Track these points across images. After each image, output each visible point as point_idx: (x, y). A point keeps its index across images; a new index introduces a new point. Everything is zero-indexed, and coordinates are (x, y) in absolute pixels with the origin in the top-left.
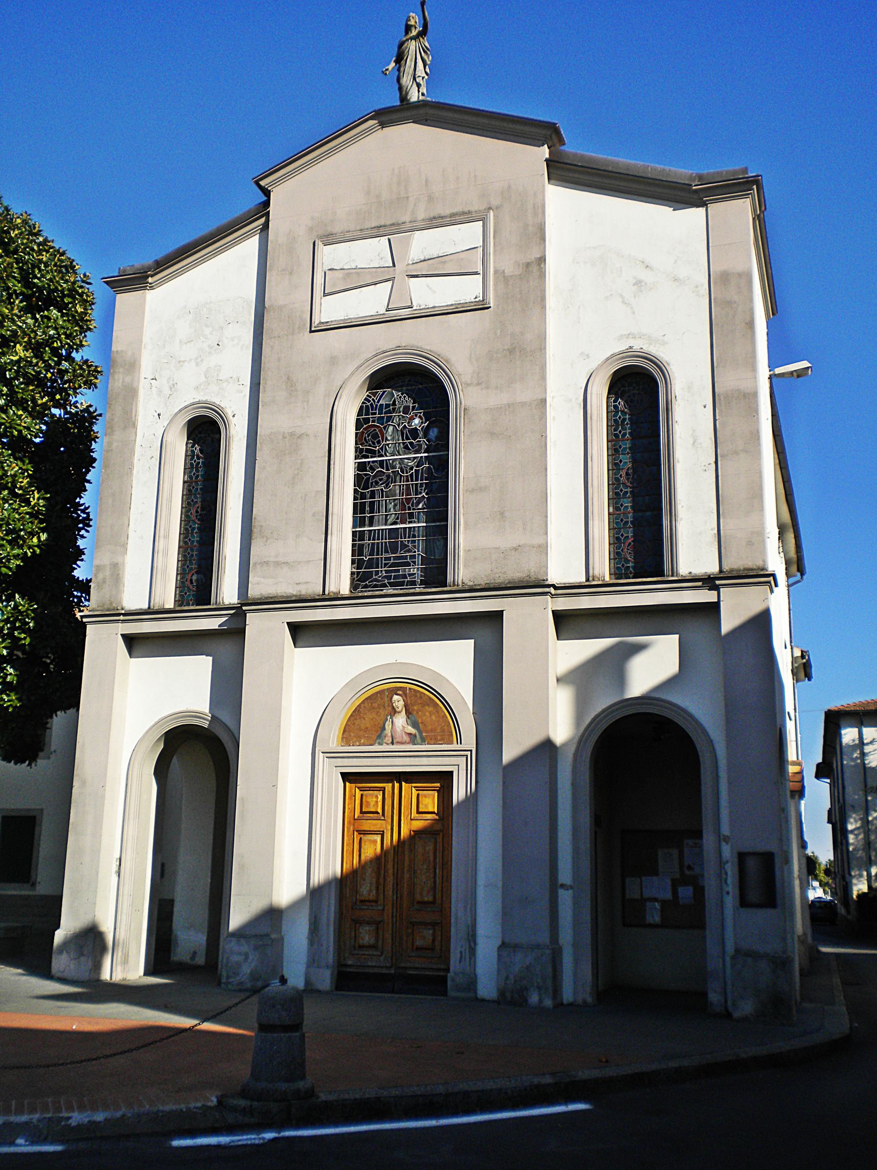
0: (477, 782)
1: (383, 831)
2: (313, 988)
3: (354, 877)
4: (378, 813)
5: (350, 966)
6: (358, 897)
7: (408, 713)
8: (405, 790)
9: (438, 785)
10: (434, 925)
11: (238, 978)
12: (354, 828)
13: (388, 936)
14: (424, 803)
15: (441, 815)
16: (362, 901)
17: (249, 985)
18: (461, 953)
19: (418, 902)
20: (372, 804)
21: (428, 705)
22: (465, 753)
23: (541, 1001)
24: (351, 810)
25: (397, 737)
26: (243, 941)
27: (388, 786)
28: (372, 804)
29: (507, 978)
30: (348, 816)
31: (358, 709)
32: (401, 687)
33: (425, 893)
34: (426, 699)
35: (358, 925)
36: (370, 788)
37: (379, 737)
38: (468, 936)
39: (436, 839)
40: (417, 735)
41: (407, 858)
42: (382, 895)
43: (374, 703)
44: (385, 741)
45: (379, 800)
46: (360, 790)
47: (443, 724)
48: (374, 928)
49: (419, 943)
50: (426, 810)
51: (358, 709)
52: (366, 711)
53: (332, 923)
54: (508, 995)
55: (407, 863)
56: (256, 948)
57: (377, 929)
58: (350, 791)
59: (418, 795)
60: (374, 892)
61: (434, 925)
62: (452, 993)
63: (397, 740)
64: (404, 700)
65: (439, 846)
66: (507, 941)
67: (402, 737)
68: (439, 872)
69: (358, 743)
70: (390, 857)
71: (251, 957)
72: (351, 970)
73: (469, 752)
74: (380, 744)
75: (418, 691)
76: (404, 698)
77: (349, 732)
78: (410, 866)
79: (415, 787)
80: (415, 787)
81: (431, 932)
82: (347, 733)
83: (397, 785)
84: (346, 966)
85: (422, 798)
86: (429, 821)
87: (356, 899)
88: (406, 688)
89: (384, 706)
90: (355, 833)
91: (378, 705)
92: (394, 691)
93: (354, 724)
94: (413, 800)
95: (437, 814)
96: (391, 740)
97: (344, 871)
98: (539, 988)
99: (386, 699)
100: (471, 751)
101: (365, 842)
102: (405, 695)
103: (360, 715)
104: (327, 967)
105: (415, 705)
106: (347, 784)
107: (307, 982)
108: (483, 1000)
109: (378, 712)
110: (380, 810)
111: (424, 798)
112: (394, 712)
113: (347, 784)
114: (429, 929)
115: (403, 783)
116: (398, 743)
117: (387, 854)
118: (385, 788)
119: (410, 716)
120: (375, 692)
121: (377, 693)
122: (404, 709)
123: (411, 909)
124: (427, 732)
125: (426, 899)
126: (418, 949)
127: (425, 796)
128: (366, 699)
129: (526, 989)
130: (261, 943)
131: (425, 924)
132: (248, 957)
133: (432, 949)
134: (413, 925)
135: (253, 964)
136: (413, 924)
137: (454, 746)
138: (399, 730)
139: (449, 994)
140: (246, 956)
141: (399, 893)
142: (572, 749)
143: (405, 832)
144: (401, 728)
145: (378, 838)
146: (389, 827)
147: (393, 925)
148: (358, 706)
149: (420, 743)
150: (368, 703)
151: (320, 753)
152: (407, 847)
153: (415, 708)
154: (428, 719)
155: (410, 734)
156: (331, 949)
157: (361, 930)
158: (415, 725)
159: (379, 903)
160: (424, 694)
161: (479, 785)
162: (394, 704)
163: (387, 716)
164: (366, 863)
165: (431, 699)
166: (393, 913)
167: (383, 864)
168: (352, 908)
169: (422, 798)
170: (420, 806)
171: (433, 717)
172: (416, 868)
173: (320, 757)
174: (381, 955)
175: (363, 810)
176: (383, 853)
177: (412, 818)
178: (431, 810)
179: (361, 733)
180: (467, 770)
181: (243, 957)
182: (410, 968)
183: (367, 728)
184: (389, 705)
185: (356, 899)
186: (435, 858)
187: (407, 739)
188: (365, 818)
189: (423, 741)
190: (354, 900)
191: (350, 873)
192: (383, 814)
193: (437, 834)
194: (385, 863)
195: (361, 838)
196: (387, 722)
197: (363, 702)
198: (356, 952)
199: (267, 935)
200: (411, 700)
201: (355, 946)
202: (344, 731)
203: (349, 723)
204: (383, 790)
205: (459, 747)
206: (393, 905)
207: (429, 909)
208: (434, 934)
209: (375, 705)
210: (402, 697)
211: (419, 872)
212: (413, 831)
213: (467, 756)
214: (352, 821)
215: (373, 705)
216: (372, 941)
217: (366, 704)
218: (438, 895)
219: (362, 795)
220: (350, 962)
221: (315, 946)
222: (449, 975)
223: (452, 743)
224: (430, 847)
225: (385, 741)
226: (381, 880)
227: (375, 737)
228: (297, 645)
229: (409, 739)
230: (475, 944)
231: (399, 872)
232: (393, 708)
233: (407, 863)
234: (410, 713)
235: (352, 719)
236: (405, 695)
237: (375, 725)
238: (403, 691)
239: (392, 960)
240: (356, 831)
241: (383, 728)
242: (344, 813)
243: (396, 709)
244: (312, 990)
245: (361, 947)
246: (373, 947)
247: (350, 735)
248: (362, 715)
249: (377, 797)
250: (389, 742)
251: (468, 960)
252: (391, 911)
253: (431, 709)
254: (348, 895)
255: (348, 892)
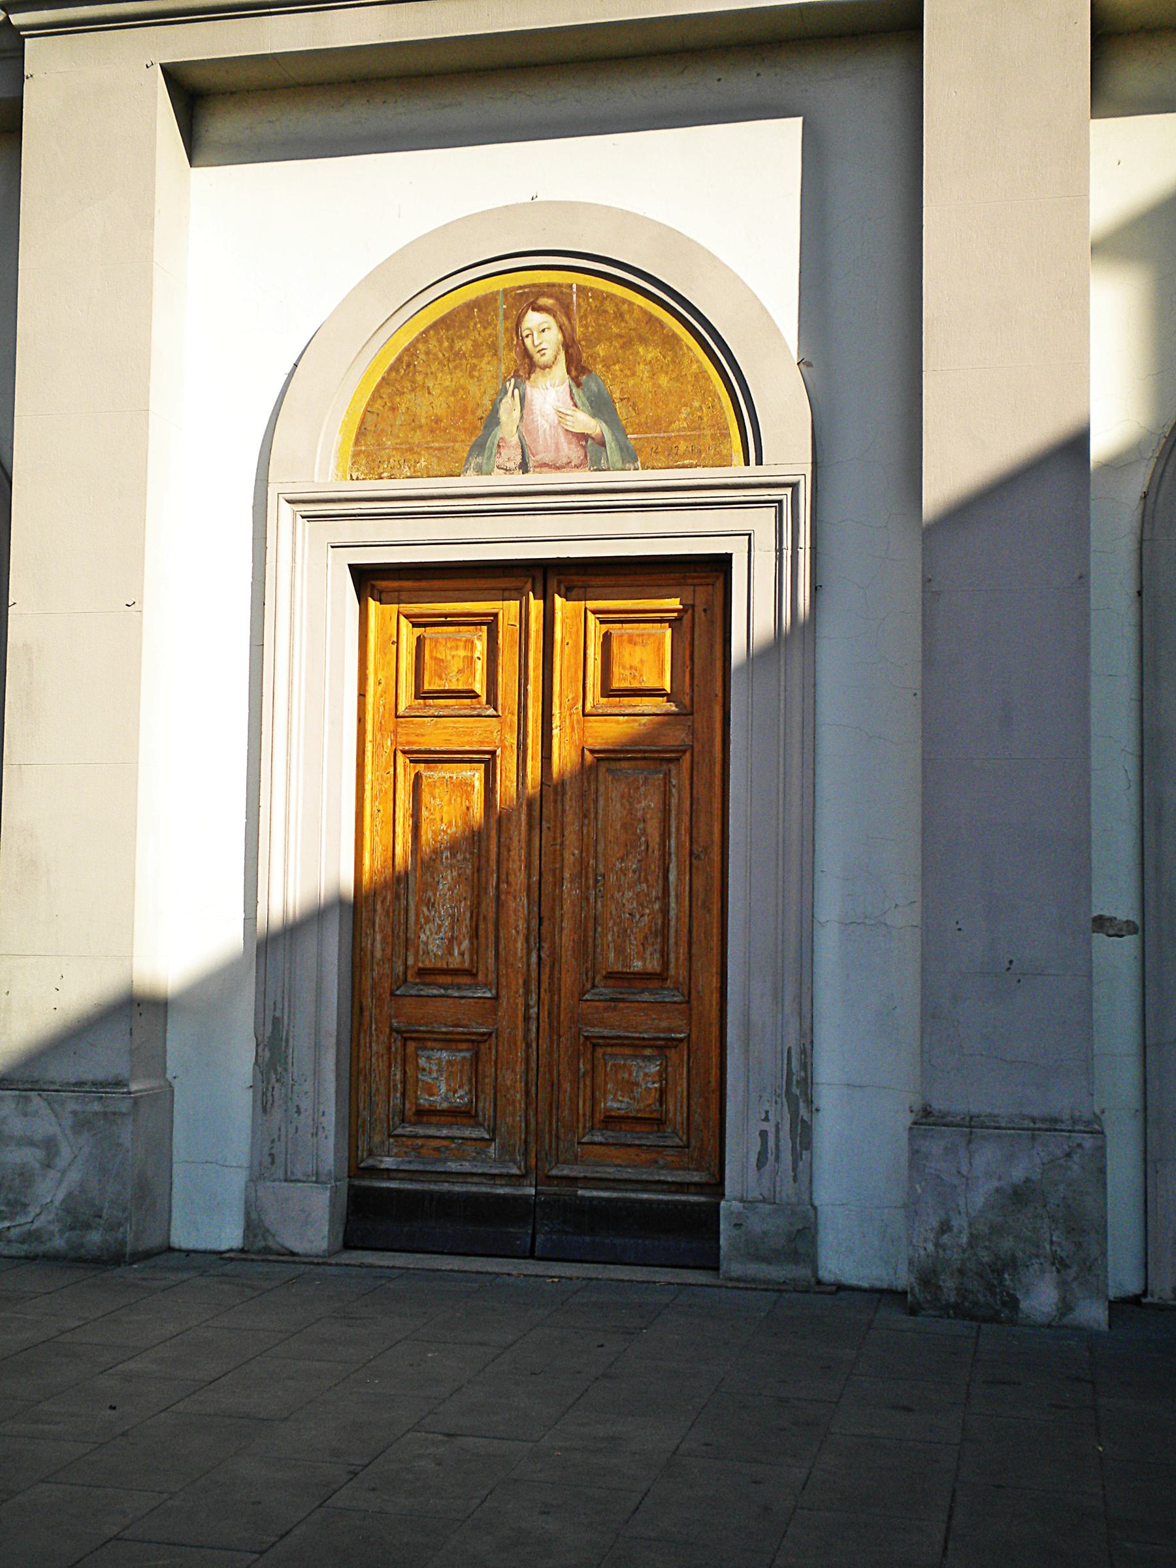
0: (815, 588)
1: (493, 753)
2: (271, 1243)
3: (397, 897)
4: (474, 696)
5: (388, 1173)
6: (411, 961)
7: (577, 368)
8: (563, 622)
9: (675, 603)
10: (663, 1046)
11: (20, 1220)
12: (395, 742)
13: (512, 1079)
14: (627, 661)
15: (687, 701)
16: (422, 972)
17: (58, 1243)
18: (763, 1134)
19: (610, 976)
20: (456, 665)
21: (643, 340)
22: (775, 494)
23: (1066, 1306)
24: (387, 684)
25: (541, 448)
26: (37, 1102)
27: (508, 610)
28: (456, 665)
29: (945, 1227)
30: (376, 710)
31: (406, 359)
32: (551, 285)
33: (632, 948)
34: (638, 321)
35: (411, 1046)
36: (446, 616)
37: (479, 447)
38: (789, 1084)
39: (667, 775)
40: (608, 437)
41: (571, 837)
42: (491, 954)
43: (461, 338)
44: (500, 461)
45: (477, 654)
46: (415, 625)
47: (696, 404)
48: (468, 1055)
49: (615, 1103)
50: (635, 685)
51: (406, 359)
52: (435, 366)
53: (330, 1042)
54: (949, 1284)
55: (571, 855)
56: (82, 1123)
57: (476, 1058)
58: (382, 629)
59: (607, 637)
60: (466, 944)
61: (663, 1046)
62: (733, 1267)
63: (538, 457)
64: (561, 327)
65: (679, 799)
66: (937, 1105)
67: (557, 449)
68: (678, 879)
69: (407, 471)
70: (518, 833)
71: (66, 1152)
72: (393, 1185)
73: (789, 491)
74: (480, 471)
75: (611, 296)
76: (564, 320)
77: (379, 434)
78: (582, 863)
79: (594, 612)
80: (594, 612)
81: (654, 1069)
82: (370, 439)
83: (536, 606)
84: (374, 1172)
85: (621, 643)
86: (644, 719)
87: (406, 968)
88: (571, 286)
89: (494, 348)
90: (401, 758)
91: (476, 345)
92: (529, 299)
93: (393, 409)
94: (590, 651)
95: (669, 697)
96: (519, 459)
97: (366, 877)
98: (1061, 1264)
99: (501, 326)
100: (794, 486)
101: (433, 785)
102: (566, 308)
103: (413, 381)
104: (318, 1179)
105: (599, 341)
106: (372, 604)
107: (252, 1226)
108: (840, 1287)
109: (474, 367)
110: (479, 687)
111: (628, 649)
112: (528, 365)
113: (372, 604)
114: (648, 1058)
115: (559, 600)
116: (543, 465)
117: (504, 821)
118: (496, 615)
119: (583, 378)
120: (460, 302)
121: (470, 306)
122: (562, 357)
123: (587, 997)
124: (640, 428)
125: (637, 965)
126: (610, 1120)
127: (631, 640)
128: (434, 326)
129: (1012, 1264)
130: (96, 1107)
131: (636, 1045)
132: (57, 1153)
133: (658, 1122)
134: (594, 1046)
135: (74, 1176)
136: (594, 1043)
137: (737, 471)
138: (547, 426)
139: (724, 1266)
140: (50, 1146)
141: (546, 945)
142: (1139, 481)
143: (564, 756)
144: (554, 418)
145: (476, 776)
146: (512, 739)
147: (528, 1046)
148: (407, 349)
149: (619, 465)
150: (440, 341)
151: (283, 503)
152: (570, 804)
153: (601, 350)
154: (648, 385)
155: (583, 437)
156: (331, 1128)
157: (422, 1062)
158: (600, 406)
159: (481, 977)
160: (631, 304)
161: (823, 596)
162: (528, 342)
163: (505, 380)
164: (436, 852)
165: (651, 319)
166: (527, 1007)
167: (493, 857)
168: (392, 994)
169: (621, 643)
170: (616, 669)
171: (663, 380)
172: (601, 869)
173: (283, 516)
174: (493, 1140)
175: (426, 687)
176: (493, 821)
177: (588, 708)
178: (650, 682)
179: (417, 437)
180: (779, 551)
181: (40, 1154)
182: (589, 1182)
183: (438, 420)
184: (509, 346)
185: (406, 968)
186: (665, 835)
187: (572, 452)
188: (432, 712)
189: (629, 457)
190: (400, 969)
191: (385, 885)
192: (492, 700)
193: (670, 760)
194: (499, 854)
195: (418, 776)
196: (507, 399)
197: (423, 337)
198: (409, 1129)
199: (119, 1083)
200: (586, 326)
201: (403, 1112)
202: (361, 433)
203: (378, 405)
204: (491, 623)
205: (752, 473)
206: (526, 983)
207: (646, 997)
208: (663, 1075)
209: (465, 346)
210: (554, 317)
211: (612, 878)
212: (592, 751)
213: (780, 502)
214: (390, 723)
215: (458, 345)
216: (460, 1098)
217: (433, 343)
218: (677, 955)
219: (420, 641)
220: (388, 1162)
221: (277, 1115)
222: (723, 1203)
223: (725, 462)
224: (649, 803)
225: (500, 461)
226: (488, 908)
227: (463, 450)
228: (193, 164)
229: (581, 453)
230: (813, 1109)
231: (548, 878)
232: (526, 354)
233: (571, 855)
234: (583, 370)
235: (386, 391)
236: (566, 308)
237: (465, 410)
238: (557, 299)
239: (526, 1153)
240: (404, 752)
241: (492, 420)
242: (362, 695)
243: (537, 357)
244: (267, 1250)
245: (424, 1114)
246: (455, 1114)
247: (381, 446)
248: (419, 378)
249: (470, 644)
250: (511, 465)
251: (787, 1157)
252: (520, 1001)
253: (652, 353)
254: (378, 954)
255: (378, 946)
